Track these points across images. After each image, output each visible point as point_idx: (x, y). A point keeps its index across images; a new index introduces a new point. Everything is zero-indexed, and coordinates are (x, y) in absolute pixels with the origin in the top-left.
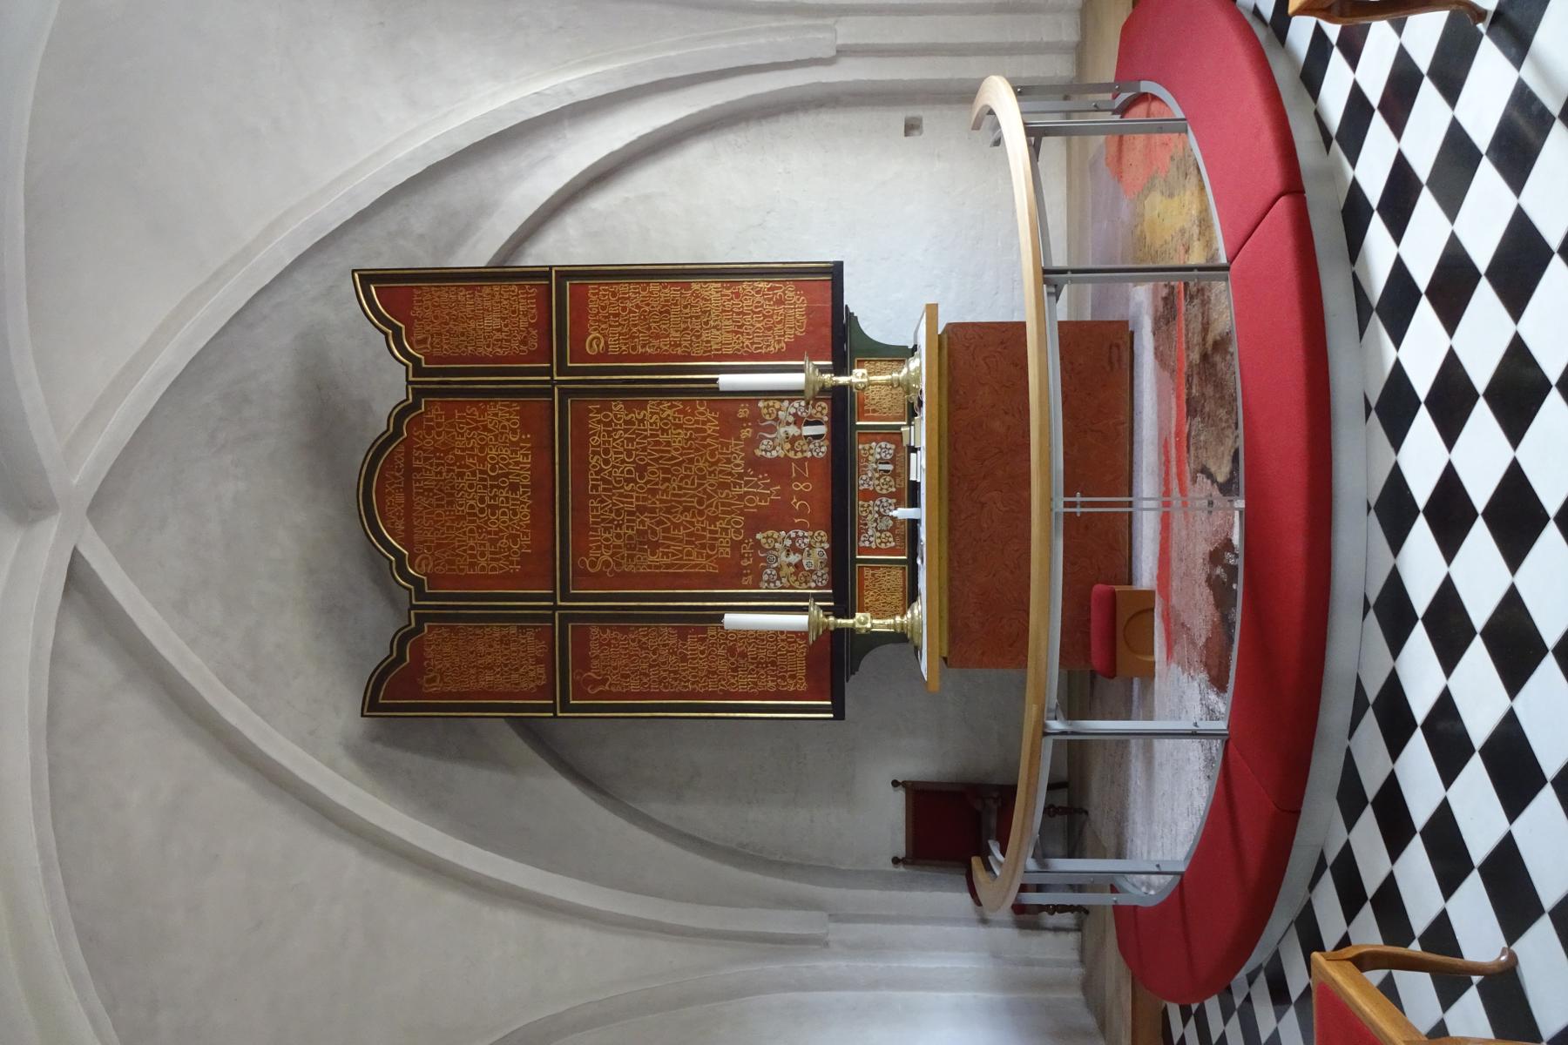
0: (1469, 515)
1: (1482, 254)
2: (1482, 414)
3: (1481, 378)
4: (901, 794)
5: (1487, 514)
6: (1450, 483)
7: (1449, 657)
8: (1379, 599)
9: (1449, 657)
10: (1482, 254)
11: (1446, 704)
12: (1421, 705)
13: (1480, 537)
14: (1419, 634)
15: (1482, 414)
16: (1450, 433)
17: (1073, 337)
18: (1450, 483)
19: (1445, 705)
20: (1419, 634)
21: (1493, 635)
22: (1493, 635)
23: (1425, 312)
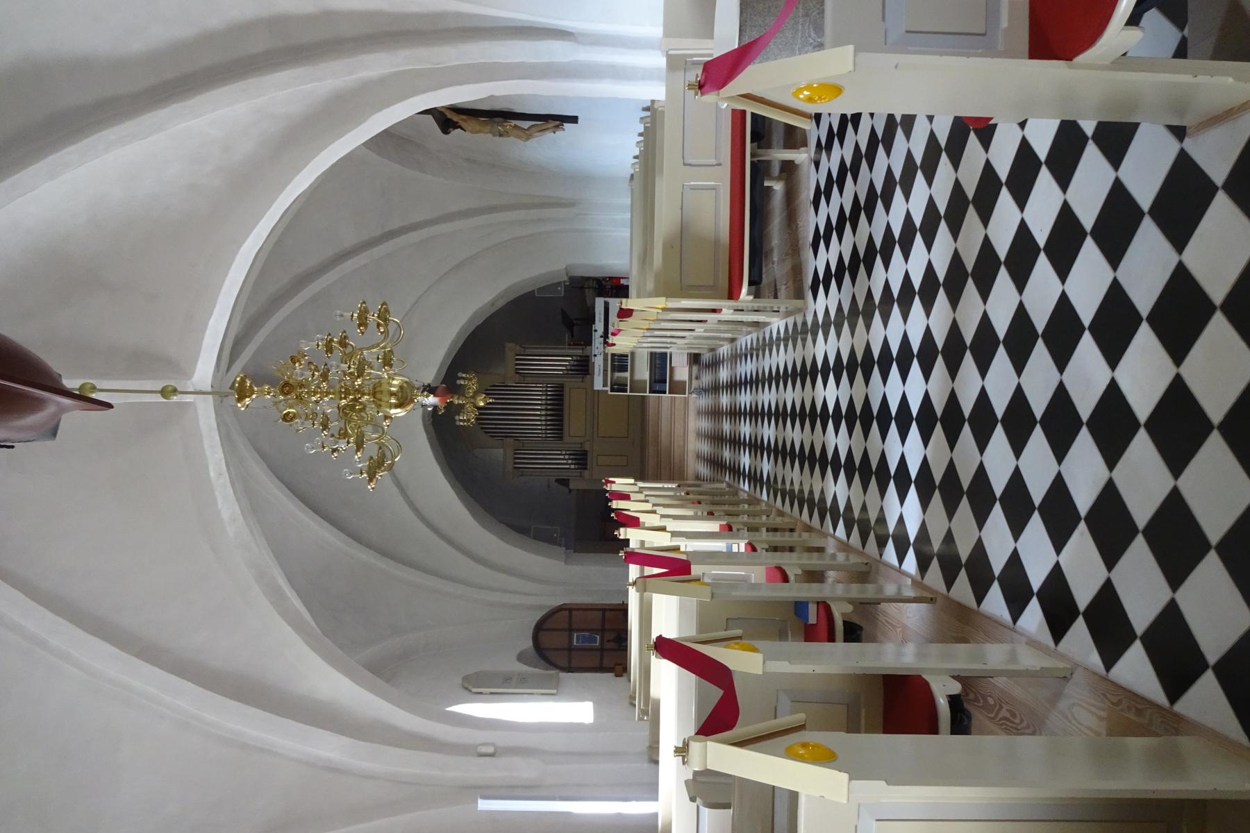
0: (1076, 424)
1: (1088, 217)
2: (1087, 344)
3: (1086, 313)
4: (854, 782)
5: (1081, 424)
6: (1061, 397)
7: (1017, 528)
8: (1043, 500)
9: (1017, 528)
10: (1088, 217)
11: (1015, 560)
12: (998, 563)
13: (1084, 444)
14: (997, 511)
15: (1087, 344)
16: (1019, 364)
17: (653, 356)
18: (1061, 397)
19: (1057, 576)
20: (997, 511)
21: (1154, 533)
22: (1154, 533)
23: (1043, 265)
